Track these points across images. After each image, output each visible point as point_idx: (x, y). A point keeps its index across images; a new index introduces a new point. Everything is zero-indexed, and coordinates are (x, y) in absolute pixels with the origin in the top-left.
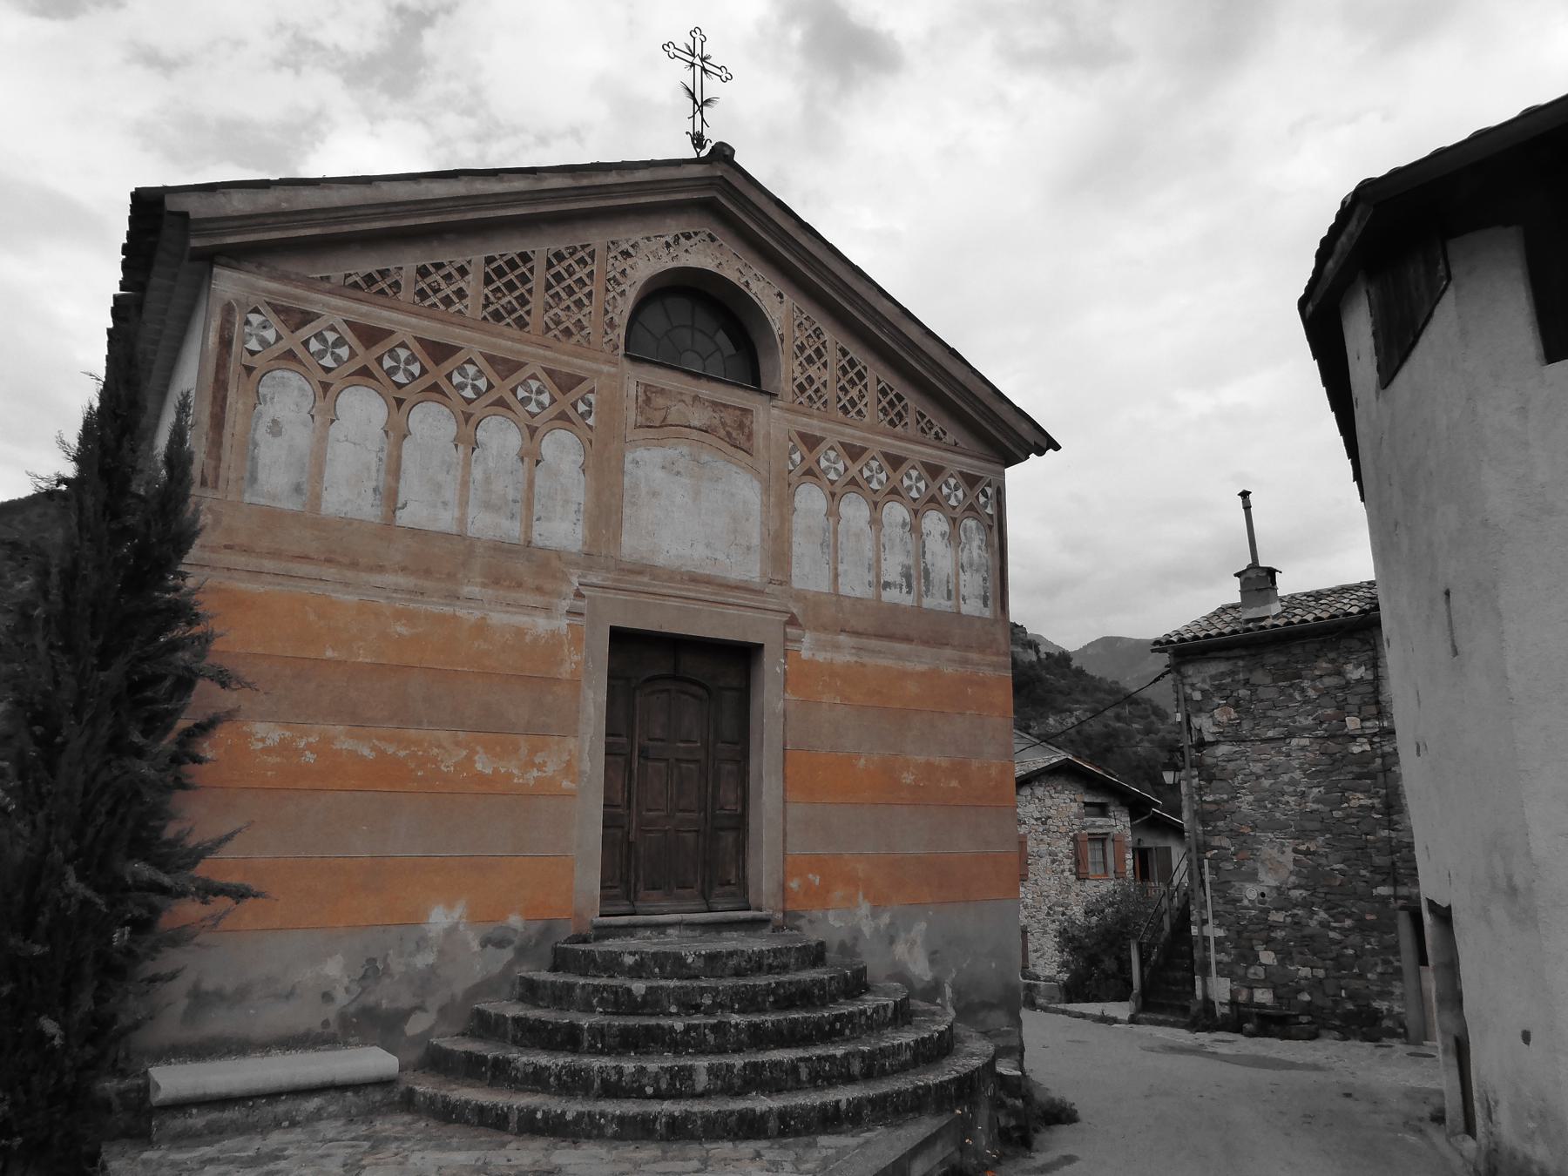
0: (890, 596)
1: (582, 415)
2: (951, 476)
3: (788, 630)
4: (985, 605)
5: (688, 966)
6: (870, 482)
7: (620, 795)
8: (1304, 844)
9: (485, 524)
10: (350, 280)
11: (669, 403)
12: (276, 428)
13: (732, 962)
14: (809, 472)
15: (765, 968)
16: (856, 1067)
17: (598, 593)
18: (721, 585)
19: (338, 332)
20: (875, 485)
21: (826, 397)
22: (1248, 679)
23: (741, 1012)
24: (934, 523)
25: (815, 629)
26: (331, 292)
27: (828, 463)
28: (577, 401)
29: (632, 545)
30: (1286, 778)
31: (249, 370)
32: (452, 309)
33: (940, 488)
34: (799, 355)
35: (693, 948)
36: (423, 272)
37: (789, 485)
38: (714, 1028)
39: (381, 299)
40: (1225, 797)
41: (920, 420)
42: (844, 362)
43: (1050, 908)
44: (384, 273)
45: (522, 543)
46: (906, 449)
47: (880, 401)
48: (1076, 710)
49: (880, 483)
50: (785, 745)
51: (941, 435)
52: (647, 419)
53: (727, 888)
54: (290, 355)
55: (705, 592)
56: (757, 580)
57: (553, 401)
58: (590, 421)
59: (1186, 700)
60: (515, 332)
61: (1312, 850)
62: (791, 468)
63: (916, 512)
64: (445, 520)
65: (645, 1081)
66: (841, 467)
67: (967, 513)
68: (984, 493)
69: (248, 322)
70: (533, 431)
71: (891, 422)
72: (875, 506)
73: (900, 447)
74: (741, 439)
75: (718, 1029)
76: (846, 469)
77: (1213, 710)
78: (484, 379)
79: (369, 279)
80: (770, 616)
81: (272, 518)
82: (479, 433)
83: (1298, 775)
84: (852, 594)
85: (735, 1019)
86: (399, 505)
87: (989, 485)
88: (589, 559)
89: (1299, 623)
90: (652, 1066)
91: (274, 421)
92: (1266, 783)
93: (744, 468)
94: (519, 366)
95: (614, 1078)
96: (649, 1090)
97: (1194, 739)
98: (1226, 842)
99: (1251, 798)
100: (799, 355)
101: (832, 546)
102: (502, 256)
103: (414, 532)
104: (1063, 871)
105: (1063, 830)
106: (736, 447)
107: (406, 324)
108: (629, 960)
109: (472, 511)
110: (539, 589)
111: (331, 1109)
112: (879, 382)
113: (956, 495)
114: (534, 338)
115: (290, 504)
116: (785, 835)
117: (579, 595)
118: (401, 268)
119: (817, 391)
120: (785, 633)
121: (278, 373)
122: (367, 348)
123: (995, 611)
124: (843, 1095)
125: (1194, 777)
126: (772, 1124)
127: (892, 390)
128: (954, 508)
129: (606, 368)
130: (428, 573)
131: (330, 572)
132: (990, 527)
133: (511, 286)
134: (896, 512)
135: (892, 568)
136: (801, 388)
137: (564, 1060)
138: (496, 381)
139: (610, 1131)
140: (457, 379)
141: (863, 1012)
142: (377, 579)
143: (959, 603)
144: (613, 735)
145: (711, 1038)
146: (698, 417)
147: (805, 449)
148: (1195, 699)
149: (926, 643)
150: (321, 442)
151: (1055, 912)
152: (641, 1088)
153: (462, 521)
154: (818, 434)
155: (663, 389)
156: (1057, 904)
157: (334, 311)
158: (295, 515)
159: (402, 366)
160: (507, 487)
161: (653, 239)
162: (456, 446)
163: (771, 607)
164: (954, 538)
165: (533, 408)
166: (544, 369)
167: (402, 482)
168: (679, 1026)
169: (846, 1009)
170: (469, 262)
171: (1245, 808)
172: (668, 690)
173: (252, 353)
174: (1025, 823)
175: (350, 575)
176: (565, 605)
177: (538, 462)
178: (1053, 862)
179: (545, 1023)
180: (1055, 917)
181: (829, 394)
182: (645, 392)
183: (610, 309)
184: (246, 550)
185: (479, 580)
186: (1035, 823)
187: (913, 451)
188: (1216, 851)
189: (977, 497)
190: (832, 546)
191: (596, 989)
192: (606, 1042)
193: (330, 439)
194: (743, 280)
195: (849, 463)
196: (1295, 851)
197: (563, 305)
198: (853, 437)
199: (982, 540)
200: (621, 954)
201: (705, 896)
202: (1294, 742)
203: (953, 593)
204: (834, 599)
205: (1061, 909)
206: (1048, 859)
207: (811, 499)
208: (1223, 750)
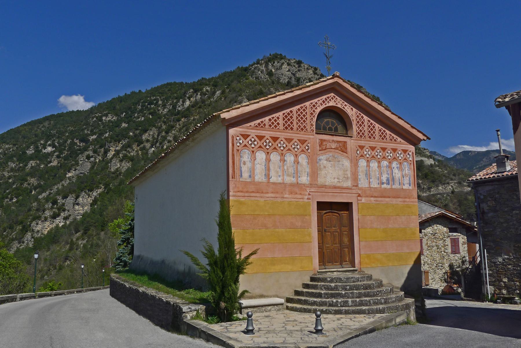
0: (384, 186)
1: (307, 150)
2: (399, 151)
3: (358, 198)
4: (410, 186)
5: (342, 280)
6: (377, 156)
7: (321, 241)
8: (517, 244)
9: (289, 180)
10: (255, 125)
11: (326, 143)
12: (244, 163)
13: (352, 280)
14: (362, 156)
15: (360, 281)
16: (383, 301)
17: (314, 194)
18: (341, 188)
19: (254, 138)
20: (379, 157)
21: (365, 134)
22: (499, 192)
23: (356, 290)
24: (395, 164)
25: (365, 197)
26: (252, 129)
27: (366, 153)
28: (306, 146)
29: (321, 181)
30: (511, 223)
31: (238, 150)
32: (277, 128)
33: (396, 155)
34: (358, 124)
35: (342, 276)
36: (270, 120)
37: (357, 160)
38: (351, 293)
39: (262, 129)
40: (491, 229)
41: (390, 136)
42: (369, 124)
43: (437, 264)
44: (262, 122)
45: (296, 183)
46: (387, 145)
47: (379, 133)
48: (451, 183)
49: (380, 156)
50: (359, 227)
51: (396, 140)
52: (322, 148)
53: (346, 263)
54: (245, 146)
55: (338, 190)
56: (350, 186)
57: (300, 147)
58: (309, 151)
59: (478, 198)
60: (291, 131)
61: (520, 246)
62: (357, 155)
63: (390, 162)
64: (280, 180)
65: (338, 303)
66: (370, 153)
67: (404, 161)
68: (409, 154)
69: (237, 139)
70: (296, 155)
71: (383, 139)
72: (379, 162)
73: (385, 145)
74: (345, 150)
75: (352, 293)
76: (371, 153)
77: (487, 202)
78: (285, 144)
79: (259, 124)
80: (354, 195)
81: (246, 183)
82: (285, 158)
83: (515, 222)
84: (374, 187)
85: (355, 291)
86: (270, 178)
87: (410, 152)
88: (311, 185)
89: (515, 174)
90: (339, 301)
91: (244, 162)
92: (505, 225)
93: (345, 157)
94: (293, 139)
95: (331, 303)
96: (339, 305)
97: (481, 211)
98: (492, 244)
99: (499, 230)
100: (358, 124)
101: (368, 175)
102: (286, 112)
103: (274, 183)
104: (441, 252)
105: (441, 237)
106: (343, 152)
107: (268, 134)
108: (329, 279)
109: (285, 177)
110: (301, 194)
111: (272, 309)
112: (379, 128)
113: (401, 156)
114: (295, 132)
115: (249, 180)
116: (360, 249)
117: (309, 194)
118: (265, 120)
119: (363, 133)
120: (358, 199)
121: (244, 150)
122: (260, 141)
123: (413, 187)
124: (381, 307)
125: (481, 223)
126: (367, 312)
127: (382, 129)
128: (400, 160)
129: (312, 137)
130: (277, 193)
131: (258, 195)
132: (411, 164)
133: (289, 120)
134: (385, 163)
135: (384, 178)
136: (359, 133)
137: (320, 300)
138: (287, 144)
139: (333, 312)
140: (279, 145)
141: (383, 290)
142: (267, 195)
143: (402, 186)
144: (319, 227)
145: (350, 295)
146: (334, 146)
147: (361, 150)
148: (481, 198)
149: (394, 197)
150: (254, 164)
151: (439, 266)
152: (337, 305)
153: (283, 179)
154: (363, 145)
155: (325, 140)
156: (439, 263)
157: (253, 133)
158: (250, 182)
159: (268, 144)
160: (291, 170)
161: (320, 100)
162: (281, 162)
163: (353, 192)
164: (400, 169)
165: (296, 150)
166: (298, 140)
167: (270, 172)
168: (343, 293)
169: (379, 290)
170: (279, 115)
171: (498, 233)
172: (330, 215)
173: (238, 146)
174: (427, 235)
175: (262, 195)
176: (306, 197)
177: (298, 163)
178: (438, 249)
179: (313, 292)
180: (439, 267)
181: (366, 134)
182: (321, 141)
183: (311, 121)
184: (242, 192)
185: (288, 193)
186: (431, 235)
187: (389, 145)
188: (488, 247)
189: (407, 156)
190: (368, 175)
191: (323, 285)
192: (328, 296)
193: (255, 164)
194: (342, 107)
195: (372, 152)
196: (514, 246)
197: (301, 122)
198: (372, 144)
199: (408, 168)
200: (327, 278)
201: (341, 264)
202: (514, 212)
203: (401, 183)
204: (369, 188)
205: (441, 265)
206: (436, 248)
207: (363, 163)
208: (491, 214)
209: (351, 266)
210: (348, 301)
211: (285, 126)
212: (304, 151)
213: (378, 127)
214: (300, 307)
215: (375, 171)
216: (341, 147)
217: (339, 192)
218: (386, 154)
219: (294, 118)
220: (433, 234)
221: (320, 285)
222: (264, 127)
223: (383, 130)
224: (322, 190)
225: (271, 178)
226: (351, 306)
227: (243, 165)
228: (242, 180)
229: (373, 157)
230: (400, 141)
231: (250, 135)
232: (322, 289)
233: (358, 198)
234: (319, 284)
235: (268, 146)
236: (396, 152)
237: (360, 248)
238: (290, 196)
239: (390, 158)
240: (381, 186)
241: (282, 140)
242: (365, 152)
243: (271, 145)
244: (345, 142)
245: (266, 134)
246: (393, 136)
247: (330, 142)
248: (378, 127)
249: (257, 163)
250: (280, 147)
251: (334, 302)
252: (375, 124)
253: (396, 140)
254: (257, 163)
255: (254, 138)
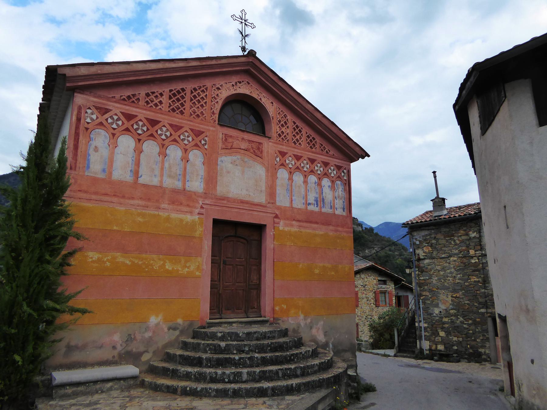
0: (310, 208)
2: (332, 166)
3: (275, 220)
4: (344, 211)
5: (240, 337)
7: (216, 277)
9: (169, 183)
10: (122, 98)
13: (255, 336)
14: (282, 165)
15: (267, 337)
16: (299, 372)
18: (251, 204)
19: (118, 116)
20: (305, 169)
21: (288, 138)
23: (259, 353)
24: (326, 182)
25: (285, 219)
26: (115, 102)
28: (201, 140)
29: (220, 190)
30: (449, 271)
31: (87, 129)
32: (158, 108)
33: (328, 170)
35: (242, 331)
36: (148, 95)
37: (275, 169)
39: (133, 104)
40: (427, 278)
42: (294, 126)
43: (366, 317)
44: (134, 95)
46: (316, 157)
47: (307, 140)
49: (307, 168)
50: (274, 260)
52: (226, 146)
53: (254, 310)
54: (101, 124)
55: (246, 206)
56: (264, 202)
57: (193, 140)
59: (414, 244)
60: (180, 116)
62: (276, 163)
63: (320, 179)
64: (155, 181)
65: (225, 377)
66: (293, 163)
67: (337, 179)
69: (86, 112)
70: (186, 150)
72: (305, 176)
74: (260, 155)
75: (251, 359)
76: (295, 164)
79: (129, 97)
80: (269, 215)
81: (95, 180)
82: (167, 151)
83: (453, 270)
85: (256, 355)
86: (139, 176)
87: (345, 169)
88: (206, 195)
90: (228, 372)
91: (96, 147)
92: (442, 273)
94: (181, 127)
95: (214, 376)
96: (226, 380)
97: (416, 258)
98: (428, 294)
100: (279, 124)
101: (290, 191)
102: (175, 89)
103: (144, 185)
104: (371, 304)
105: (371, 289)
107: (142, 113)
108: (219, 335)
109: (165, 178)
110: (188, 206)
111: (115, 387)
112: (307, 133)
113: (333, 173)
114: (186, 118)
115: (101, 176)
116: (274, 291)
117: (202, 207)
118: (140, 94)
119: (285, 136)
120: (274, 221)
121: (97, 130)
123: (347, 213)
124: (294, 382)
125: (416, 271)
126: (269, 392)
127: (311, 136)
129: (211, 128)
130: (149, 200)
131: (115, 200)
132: (346, 184)
133: (178, 100)
134: (312, 179)
136: (280, 135)
138: (173, 133)
139: (213, 394)
140: (159, 132)
141: (301, 353)
142: (132, 202)
145: (248, 362)
146: (244, 145)
152: (224, 379)
153: (161, 181)
155: (231, 136)
157: (116, 108)
158: (103, 180)
159: (140, 127)
161: (228, 83)
162: (159, 155)
163: (269, 212)
164: (333, 188)
165: (186, 142)
166: (190, 129)
167: (140, 168)
168: (237, 357)
170: (164, 91)
171: (434, 282)
173: (88, 123)
175: (122, 200)
177: (188, 161)
178: (367, 300)
181: (289, 137)
184: (86, 192)
187: (318, 157)
189: (341, 173)
190: (290, 191)
191: (208, 345)
194: (259, 98)
195: (296, 161)
196: (452, 297)
197: (196, 106)
198: (297, 152)
199: (342, 188)
202: (452, 259)
203: (333, 207)
204: (291, 209)
205: (370, 317)
206: (366, 299)
207: (283, 174)
208: (427, 261)
209: (246, 316)
210: (241, 373)
211: (171, 108)
212: (199, 146)
213: (306, 132)
214: (161, 383)
215: (299, 187)
216: (254, 149)
217: (247, 208)
218: (315, 168)
219: (187, 98)
220: (363, 285)
221: (204, 344)
222: (136, 102)
223: (312, 137)
224: (223, 203)
225: (141, 177)
226: (246, 382)
227: (94, 152)
228: (89, 174)
229: (298, 168)
230: (333, 155)
231: (111, 110)
232: (205, 352)
233: (275, 220)
234: (203, 342)
235: (140, 130)
236: (328, 167)
237: (274, 289)
238: (171, 206)
239: (320, 173)
240: (307, 208)
241: (164, 126)
242: (287, 160)
243: (145, 130)
244: (260, 143)
245: (139, 113)
246: (324, 147)
247: (239, 140)
248: (306, 132)
249: (119, 153)
250: (161, 135)
251: (219, 374)
252: (302, 128)
253: (328, 152)
254: (119, 153)
255: (118, 116)
